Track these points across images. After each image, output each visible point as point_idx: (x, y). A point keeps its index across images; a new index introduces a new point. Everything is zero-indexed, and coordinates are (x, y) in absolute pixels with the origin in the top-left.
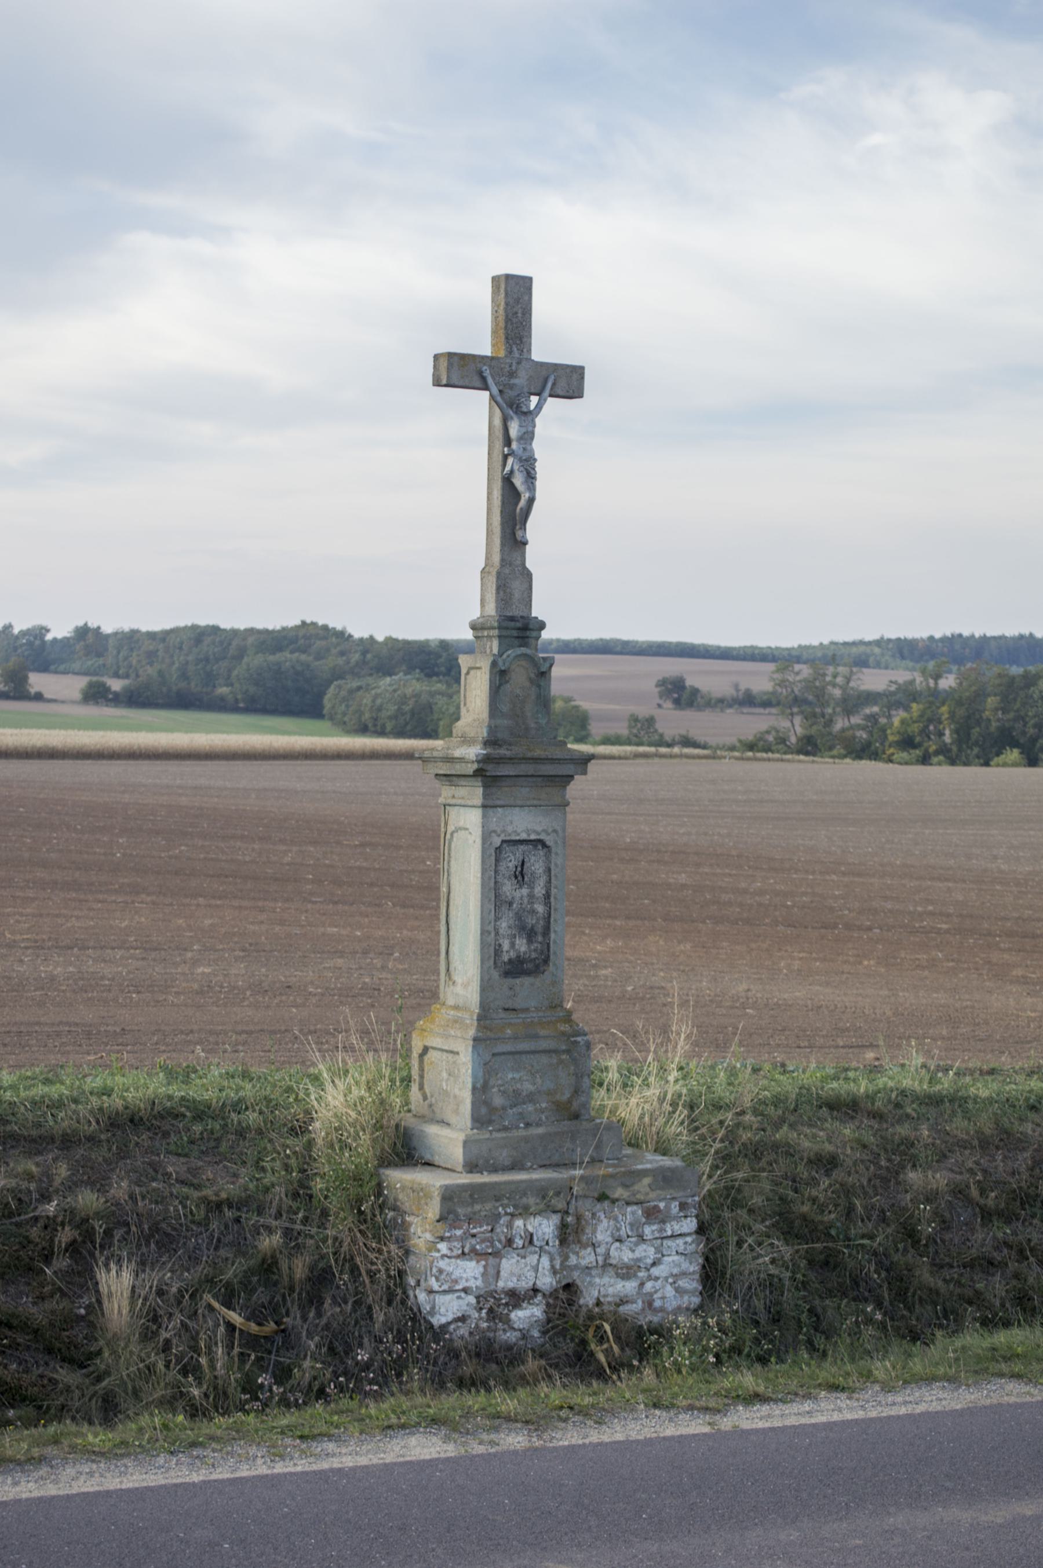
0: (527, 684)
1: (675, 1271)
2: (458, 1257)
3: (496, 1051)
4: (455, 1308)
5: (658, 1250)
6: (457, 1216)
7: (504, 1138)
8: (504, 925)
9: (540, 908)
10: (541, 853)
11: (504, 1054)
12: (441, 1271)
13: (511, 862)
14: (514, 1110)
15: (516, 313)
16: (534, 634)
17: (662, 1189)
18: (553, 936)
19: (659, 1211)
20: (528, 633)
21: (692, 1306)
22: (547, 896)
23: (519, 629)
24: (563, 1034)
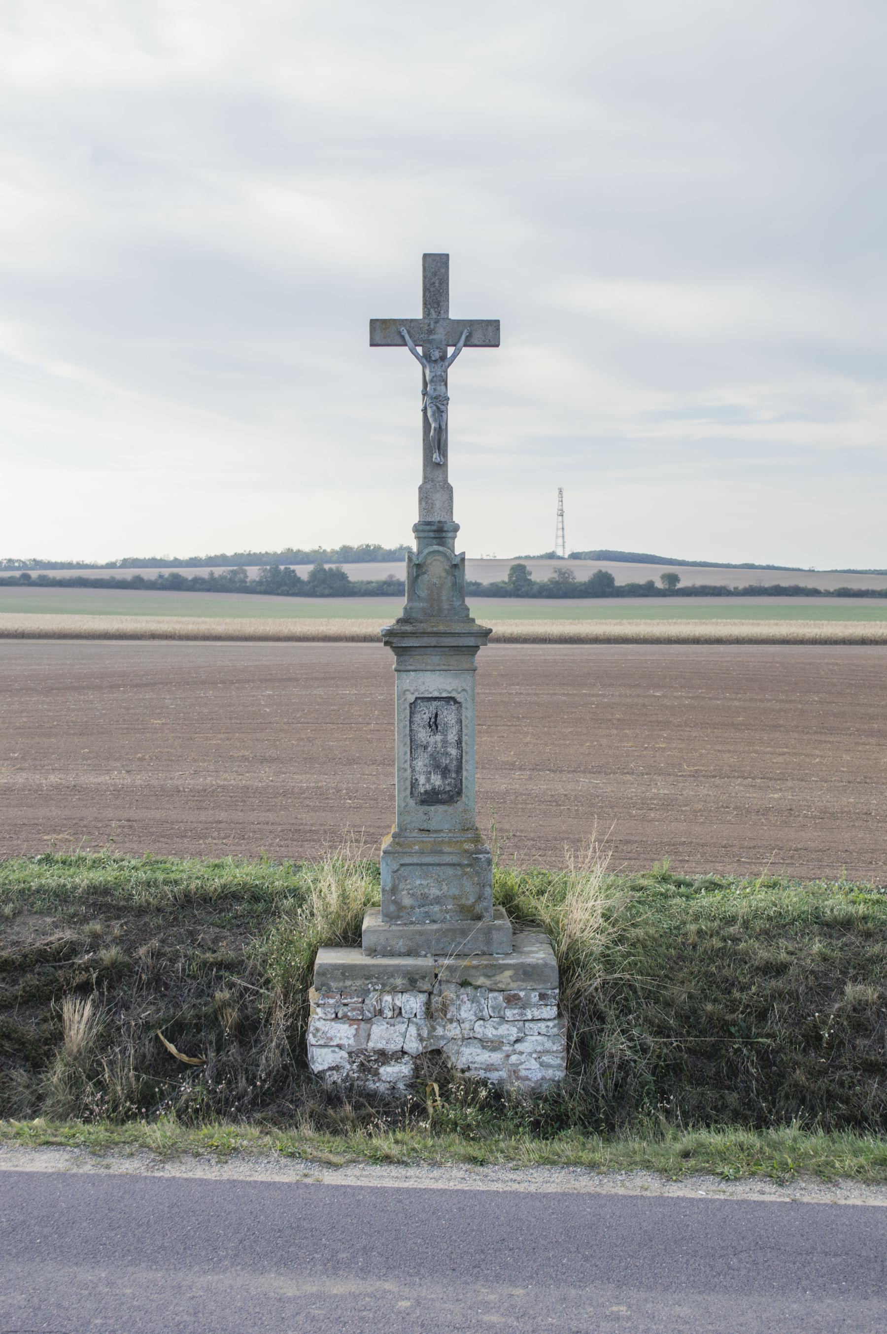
0: (444, 574)
1: (539, 1048)
2: (333, 1019)
3: (403, 862)
4: (330, 1061)
5: (520, 1030)
6: (329, 989)
7: (400, 931)
8: (419, 764)
9: (453, 752)
10: (453, 707)
11: (410, 864)
12: (317, 1030)
13: (424, 714)
14: (422, 909)
15: (434, 283)
16: (450, 535)
17: (523, 981)
18: (464, 773)
19: (519, 999)
20: (444, 534)
21: (556, 1079)
22: (459, 742)
23: (434, 531)
24: (466, 851)
